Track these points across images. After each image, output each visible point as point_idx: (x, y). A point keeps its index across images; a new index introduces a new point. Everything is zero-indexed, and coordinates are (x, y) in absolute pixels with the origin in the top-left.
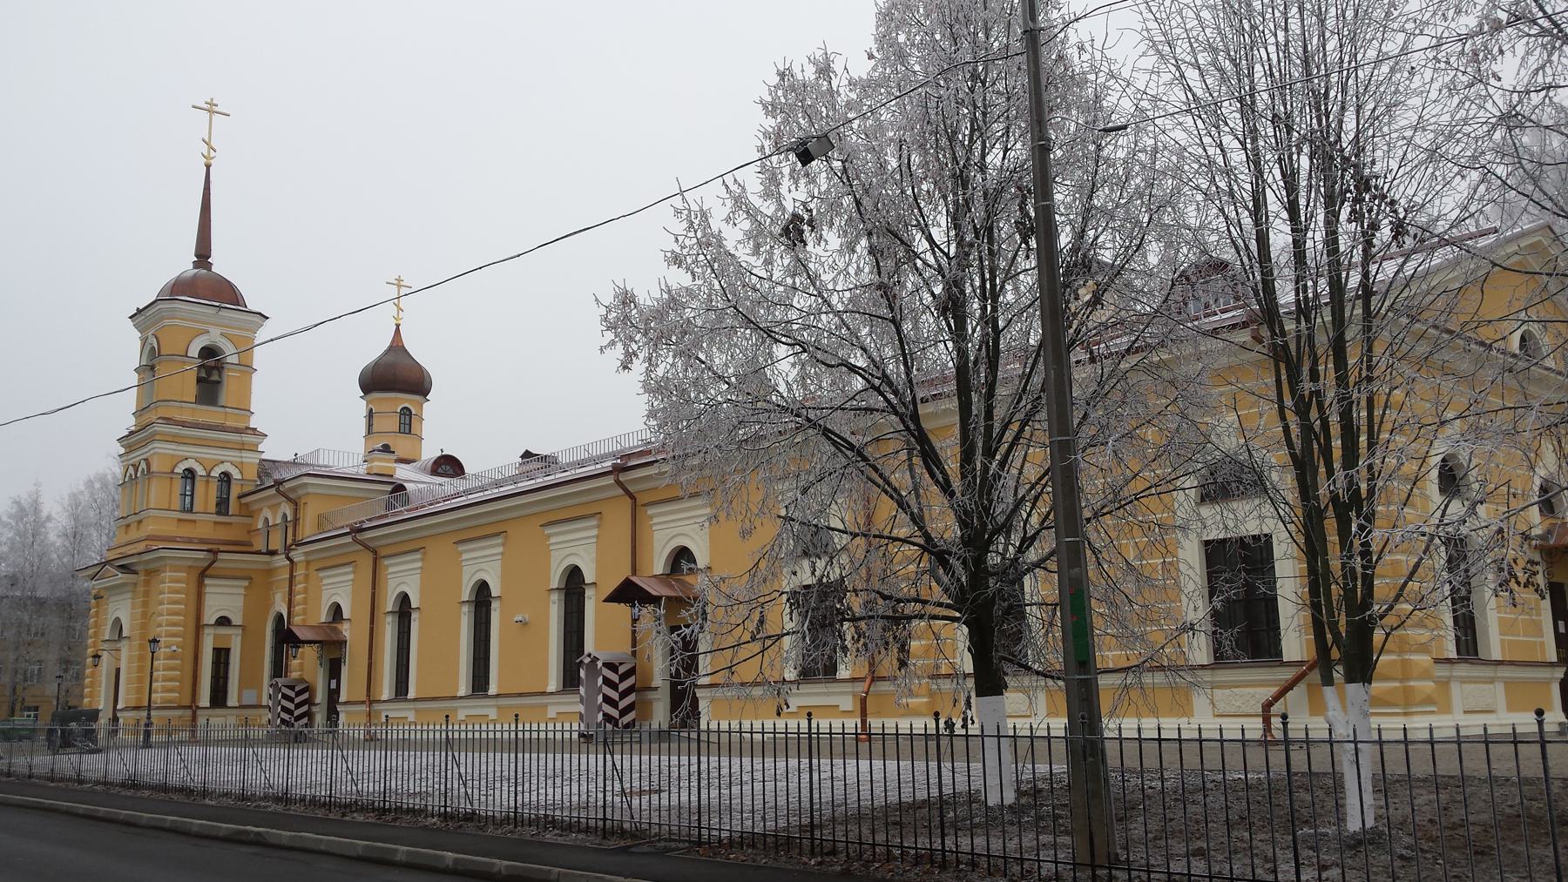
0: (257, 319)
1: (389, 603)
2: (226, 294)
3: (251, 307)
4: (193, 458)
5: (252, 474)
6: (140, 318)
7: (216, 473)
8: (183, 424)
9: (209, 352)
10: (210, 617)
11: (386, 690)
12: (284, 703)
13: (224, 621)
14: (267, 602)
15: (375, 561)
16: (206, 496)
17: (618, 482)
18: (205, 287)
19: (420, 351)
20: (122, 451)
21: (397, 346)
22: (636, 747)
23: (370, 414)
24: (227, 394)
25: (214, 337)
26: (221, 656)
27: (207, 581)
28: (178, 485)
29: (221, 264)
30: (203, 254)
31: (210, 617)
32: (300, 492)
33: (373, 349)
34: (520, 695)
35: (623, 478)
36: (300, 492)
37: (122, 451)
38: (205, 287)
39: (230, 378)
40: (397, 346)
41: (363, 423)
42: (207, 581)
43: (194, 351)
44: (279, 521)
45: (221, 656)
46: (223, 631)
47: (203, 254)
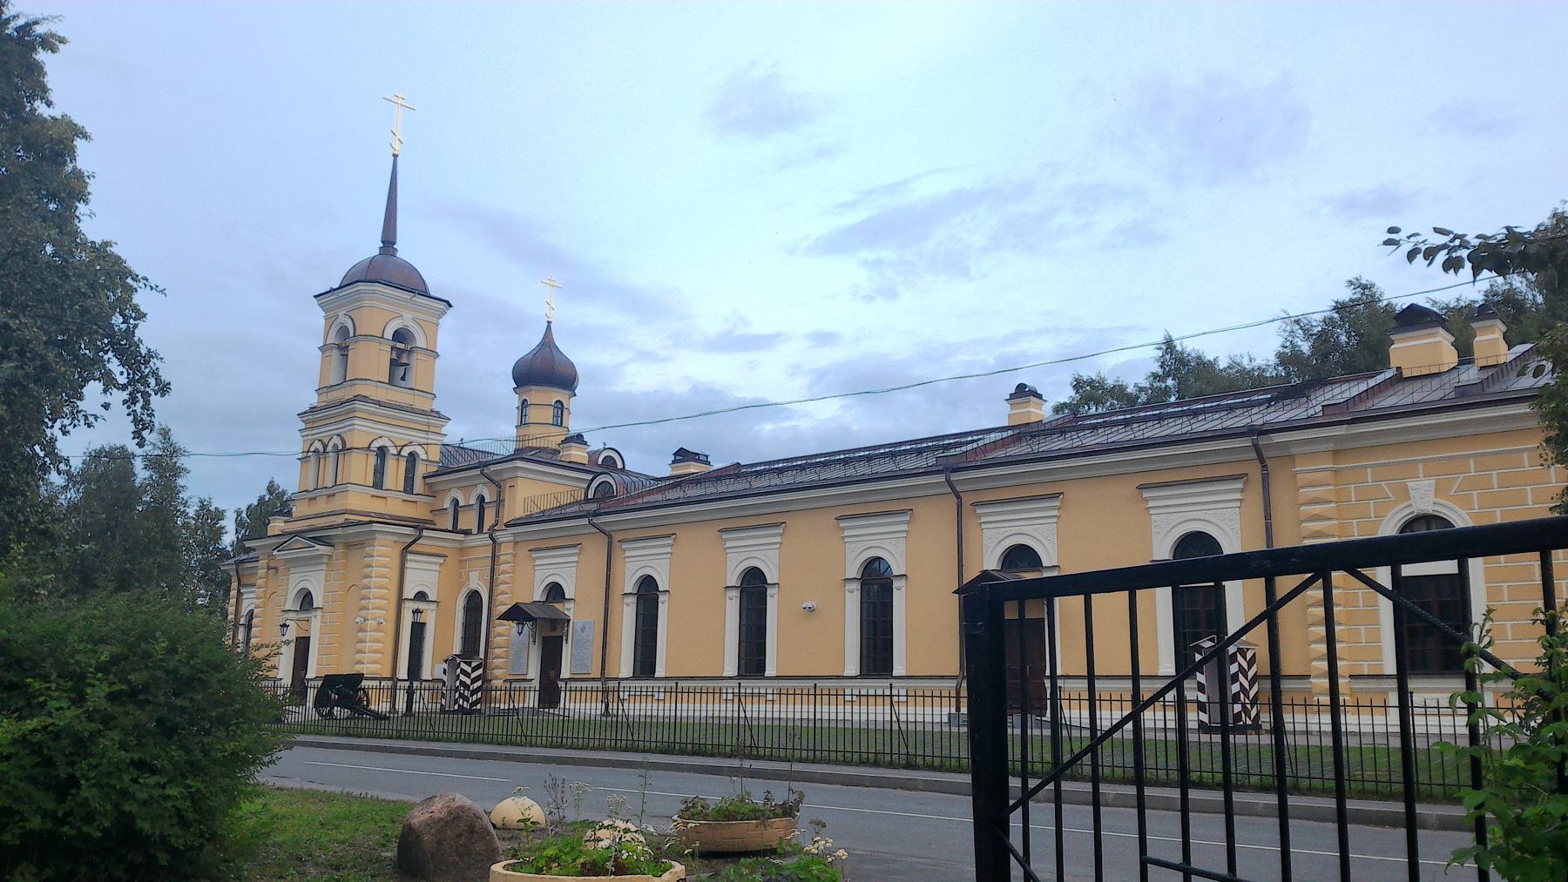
0: (442, 306)
1: (628, 581)
2: (413, 285)
3: (433, 294)
4: (390, 436)
5: (435, 454)
6: (324, 299)
7: (405, 452)
8: (379, 403)
9: (400, 336)
10: (409, 592)
11: (624, 665)
12: (462, 677)
13: (421, 596)
14: (462, 579)
15: (610, 544)
16: (395, 473)
17: (948, 481)
18: (386, 272)
19: (569, 348)
20: (303, 426)
21: (547, 343)
22: (864, 726)
23: (524, 404)
24: (416, 377)
25: (406, 320)
26: (418, 629)
27: (409, 557)
28: (373, 460)
29: (405, 250)
30: (388, 242)
31: (409, 592)
32: (506, 476)
33: (529, 342)
34: (942, 677)
35: (954, 477)
36: (506, 476)
37: (303, 426)
38: (386, 272)
39: (417, 362)
40: (547, 343)
41: (515, 415)
42: (409, 557)
43: (389, 335)
44: (473, 501)
45: (418, 629)
46: (421, 605)
47: (388, 242)
